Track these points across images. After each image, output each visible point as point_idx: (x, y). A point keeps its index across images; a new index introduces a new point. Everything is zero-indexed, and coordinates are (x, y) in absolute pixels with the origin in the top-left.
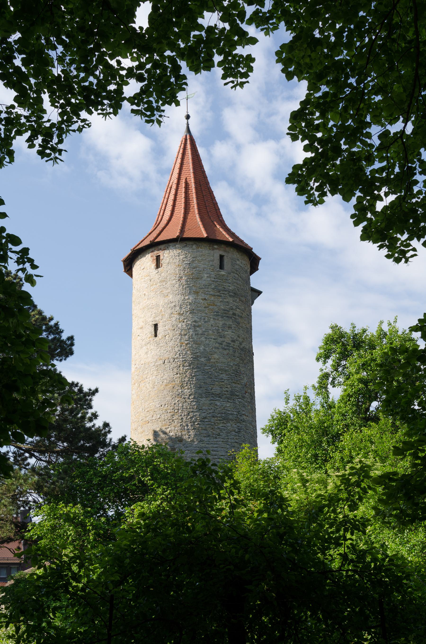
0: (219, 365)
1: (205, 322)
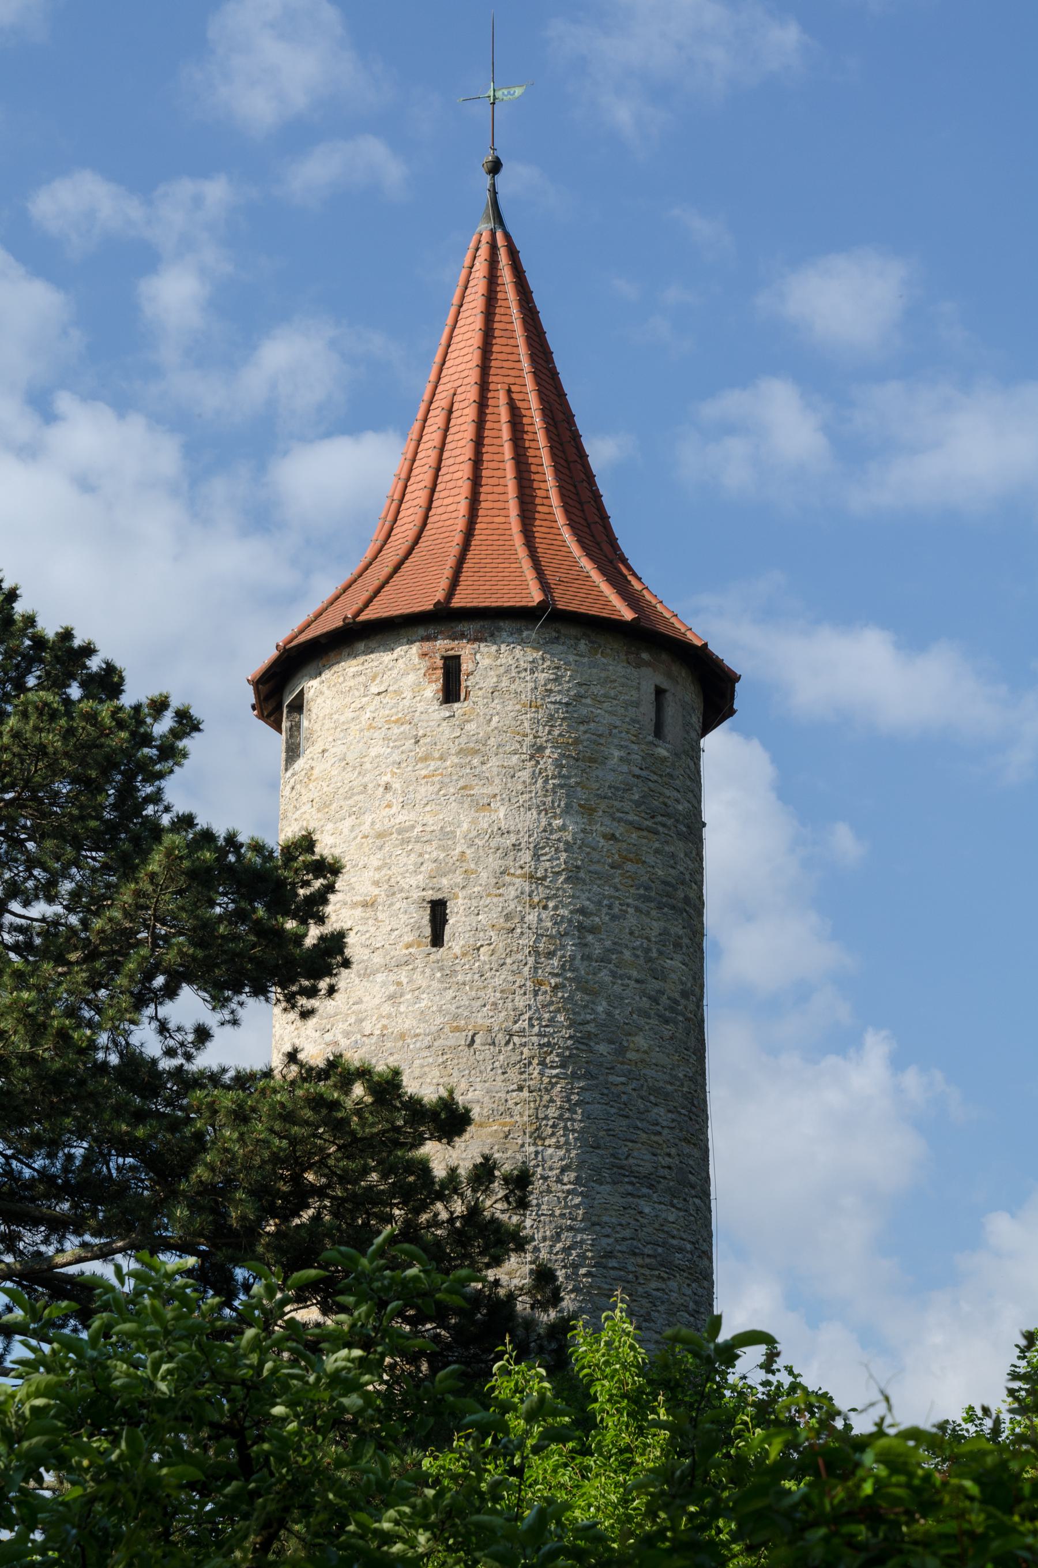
0: (649, 1072)
1: (614, 918)
